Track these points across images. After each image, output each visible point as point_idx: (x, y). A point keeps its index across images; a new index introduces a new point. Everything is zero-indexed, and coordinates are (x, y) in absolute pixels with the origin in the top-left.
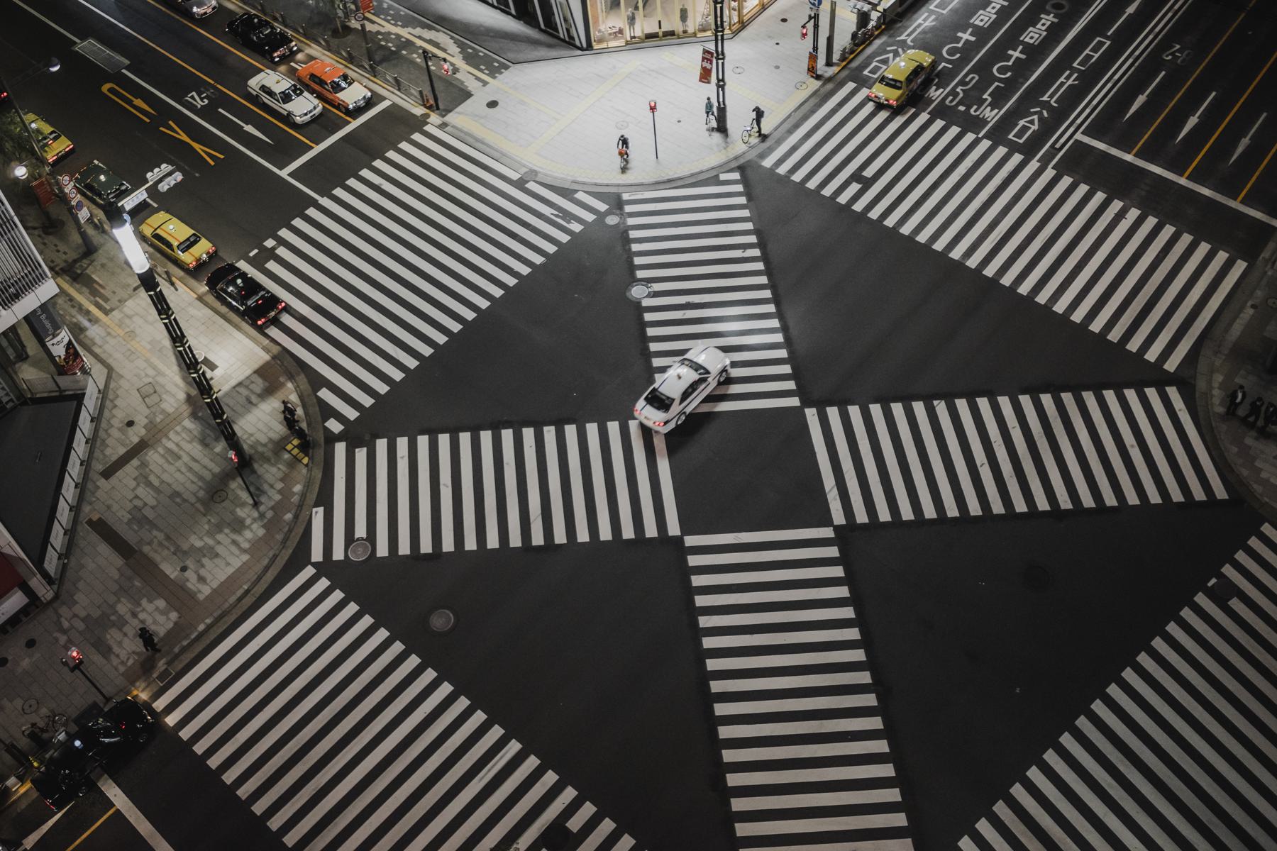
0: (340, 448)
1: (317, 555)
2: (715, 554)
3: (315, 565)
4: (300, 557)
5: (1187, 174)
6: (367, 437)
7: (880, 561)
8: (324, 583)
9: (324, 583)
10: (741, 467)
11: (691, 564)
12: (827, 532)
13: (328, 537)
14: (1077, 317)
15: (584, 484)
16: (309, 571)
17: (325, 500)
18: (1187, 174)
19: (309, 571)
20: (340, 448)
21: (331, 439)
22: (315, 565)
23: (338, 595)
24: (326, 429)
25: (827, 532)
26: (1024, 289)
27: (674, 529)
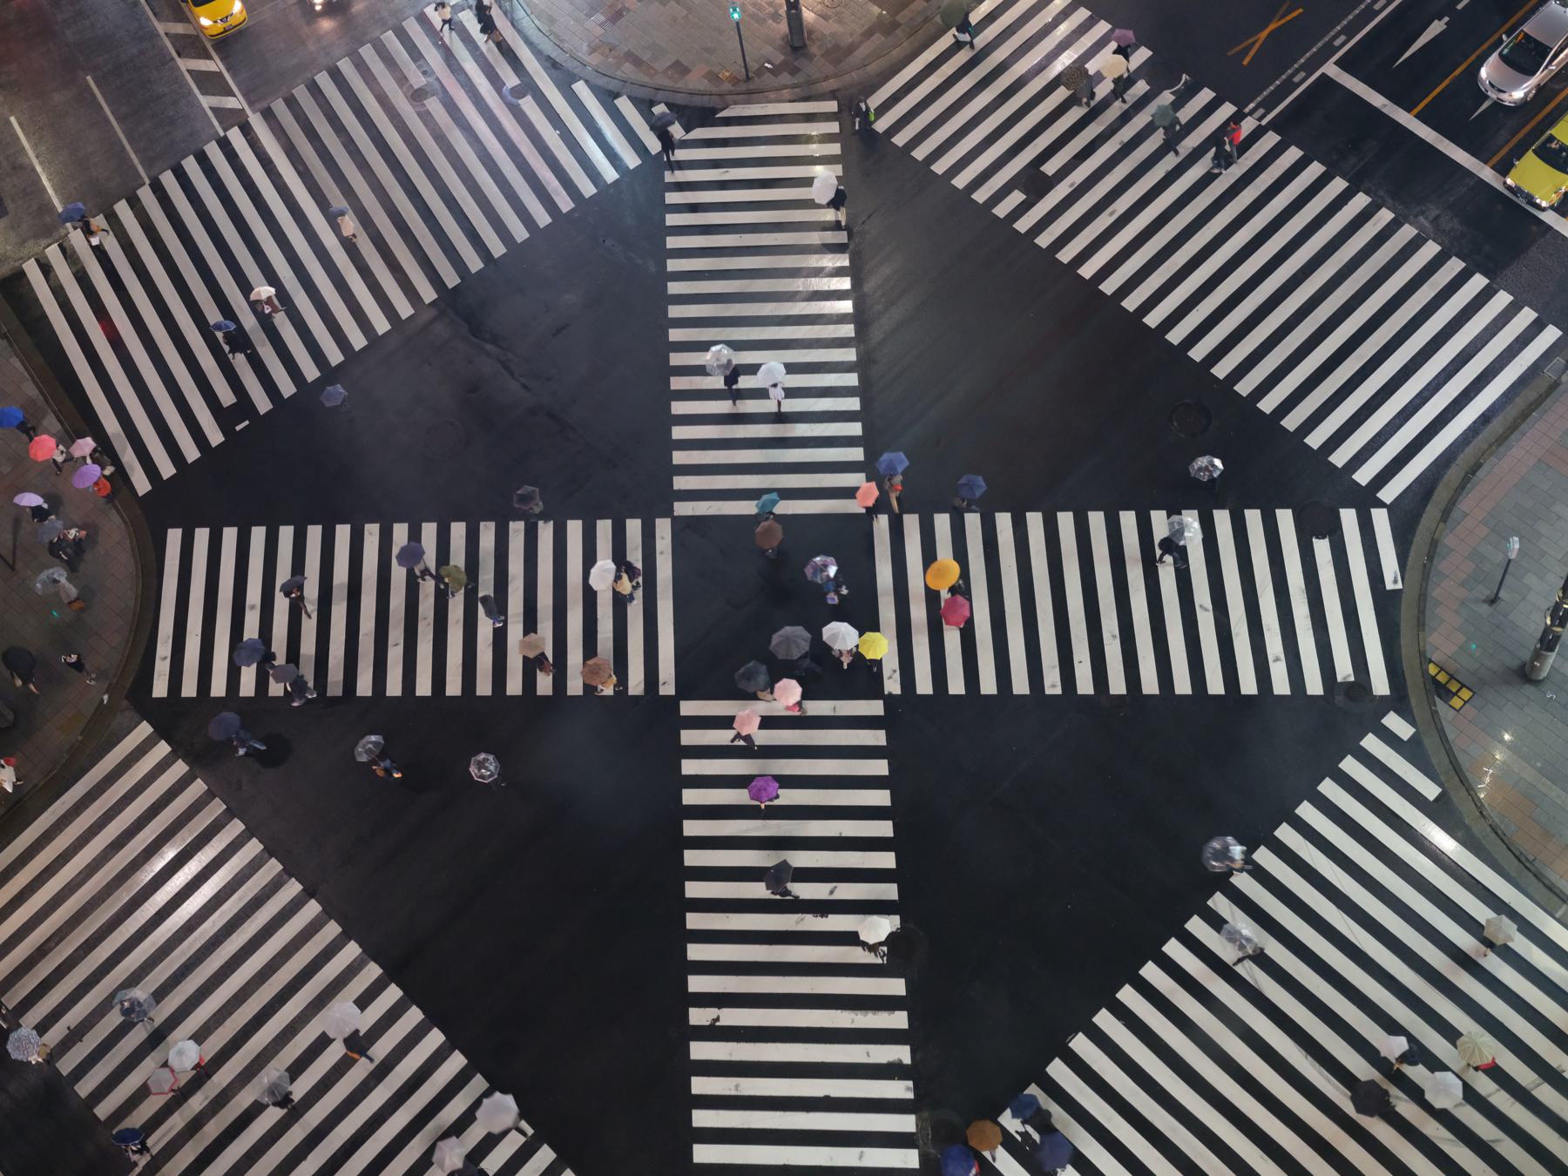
0: (1380, 685)
1: (1380, 518)
2: (829, 472)
3: (1381, 504)
4: (1406, 517)
5: (1416, 111)
6: (1340, 699)
7: (936, 745)
8: (1363, 476)
9: (1363, 476)
10: (761, 600)
11: (861, 450)
12: (875, 708)
13: (1370, 546)
14: (1244, 387)
15: (579, 602)
16: (1388, 494)
17: (1385, 601)
18: (1416, 111)
19: (1388, 494)
20: (1380, 685)
21: (1399, 701)
22: (1381, 504)
23: (1339, 458)
24: (1412, 722)
25: (875, 708)
26: (1153, 319)
27: (667, 688)
